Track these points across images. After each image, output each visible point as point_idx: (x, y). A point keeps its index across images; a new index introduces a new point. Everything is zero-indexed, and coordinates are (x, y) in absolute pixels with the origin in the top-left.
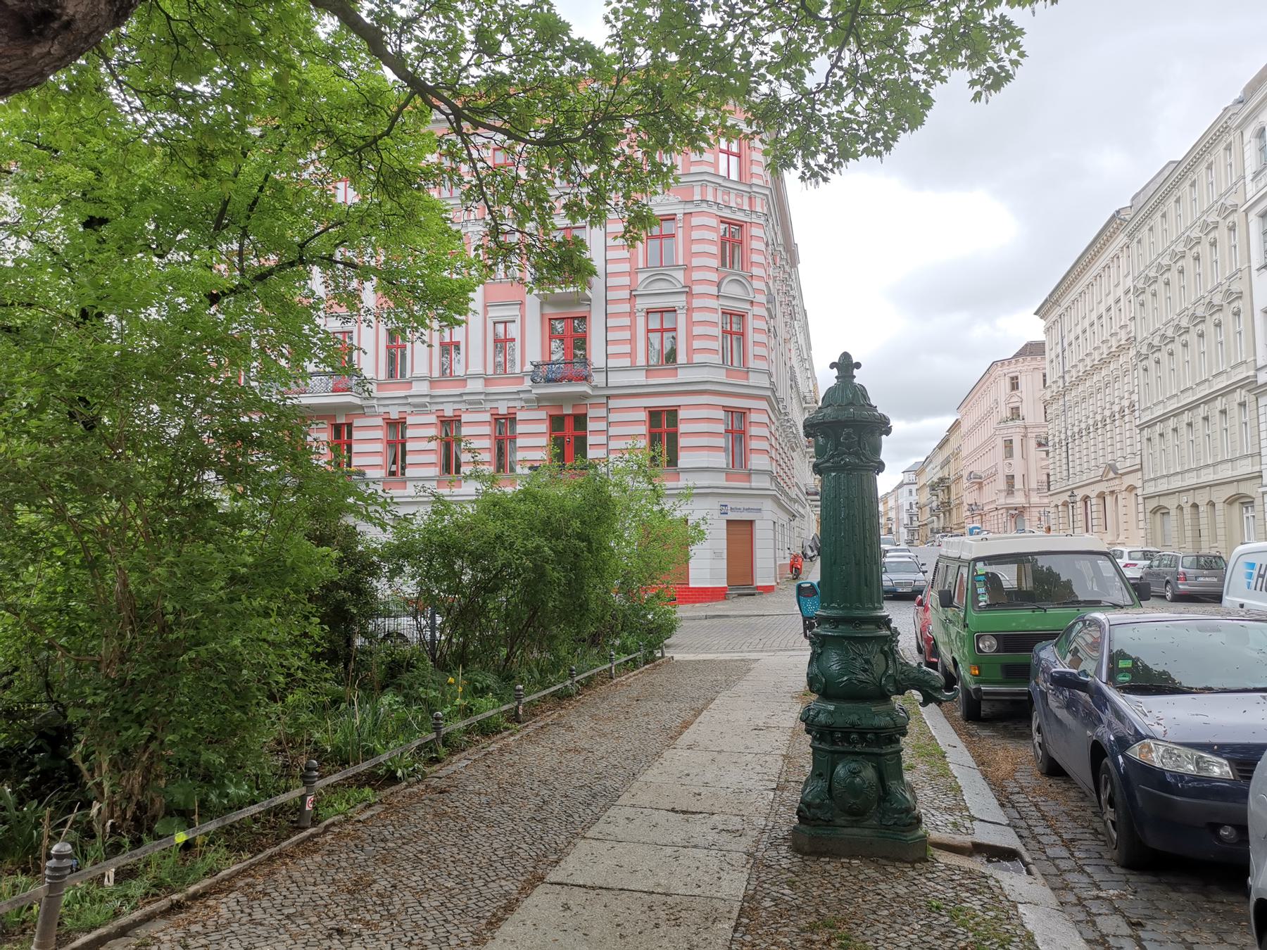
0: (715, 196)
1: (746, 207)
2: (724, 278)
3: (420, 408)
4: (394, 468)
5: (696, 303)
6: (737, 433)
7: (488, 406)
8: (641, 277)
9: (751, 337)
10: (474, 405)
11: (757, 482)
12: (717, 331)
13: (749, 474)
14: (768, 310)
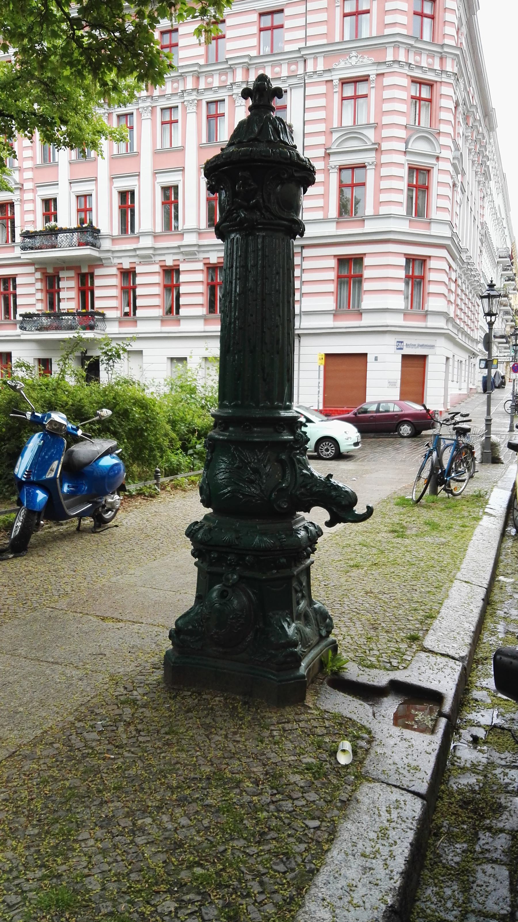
0: (407, 57)
1: (437, 67)
2: (411, 137)
3: (147, 260)
4: (127, 309)
5: (385, 158)
6: (416, 271)
7: (202, 256)
8: (335, 136)
9: (435, 189)
10: (190, 254)
11: (433, 322)
12: (403, 185)
13: (426, 315)
14: (454, 165)
